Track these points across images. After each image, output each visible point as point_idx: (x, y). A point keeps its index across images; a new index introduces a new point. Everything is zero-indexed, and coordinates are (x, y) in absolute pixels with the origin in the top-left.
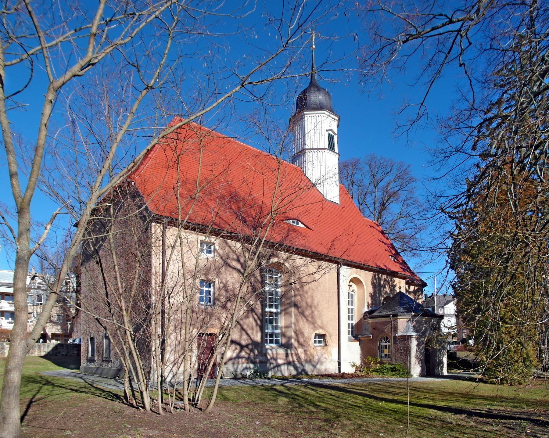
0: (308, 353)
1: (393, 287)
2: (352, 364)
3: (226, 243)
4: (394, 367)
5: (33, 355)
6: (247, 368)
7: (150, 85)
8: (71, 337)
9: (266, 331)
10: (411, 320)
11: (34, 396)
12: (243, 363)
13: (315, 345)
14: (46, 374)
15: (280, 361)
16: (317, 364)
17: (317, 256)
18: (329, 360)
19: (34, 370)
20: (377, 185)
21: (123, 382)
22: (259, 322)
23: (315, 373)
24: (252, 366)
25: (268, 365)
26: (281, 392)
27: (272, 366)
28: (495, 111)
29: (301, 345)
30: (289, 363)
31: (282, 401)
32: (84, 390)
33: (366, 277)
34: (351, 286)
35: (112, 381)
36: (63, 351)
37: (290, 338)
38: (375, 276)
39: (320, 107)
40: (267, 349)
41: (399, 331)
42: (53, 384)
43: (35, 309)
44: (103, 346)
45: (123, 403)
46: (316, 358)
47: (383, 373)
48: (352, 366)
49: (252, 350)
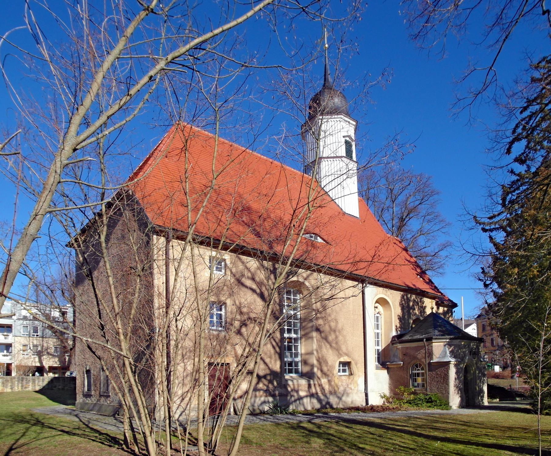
0: (333, 383)
1: (423, 309)
2: (382, 395)
3: (240, 259)
4: (430, 398)
5: (27, 389)
6: (264, 402)
7: (151, 7)
8: (69, 370)
9: (286, 359)
10: (449, 345)
11: (17, 440)
12: (261, 396)
13: (339, 374)
14: (38, 411)
15: (302, 394)
16: (343, 395)
17: (341, 274)
18: (355, 391)
19: (25, 407)
20: (395, 199)
21: (122, 420)
22: (278, 349)
23: (341, 406)
24: (271, 399)
25: (289, 398)
26: (311, 431)
27: (293, 399)
28: (535, 108)
29: (325, 374)
30: (312, 396)
31: (315, 442)
32: (77, 432)
33: (394, 298)
34: (377, 307)
35: (111, 420)
36: (59, 385)
37: (312, 366)
38: (403, 297)
39: (335, 111)
40: (287, 380)
41: (434, 357)
42: (43, 424)
43: (31, 341)
44: (100, 379)
45: (123, 449)
46: (341, 389)
47: (417, 405)
48: (382, 397)
49: (271, 382)
